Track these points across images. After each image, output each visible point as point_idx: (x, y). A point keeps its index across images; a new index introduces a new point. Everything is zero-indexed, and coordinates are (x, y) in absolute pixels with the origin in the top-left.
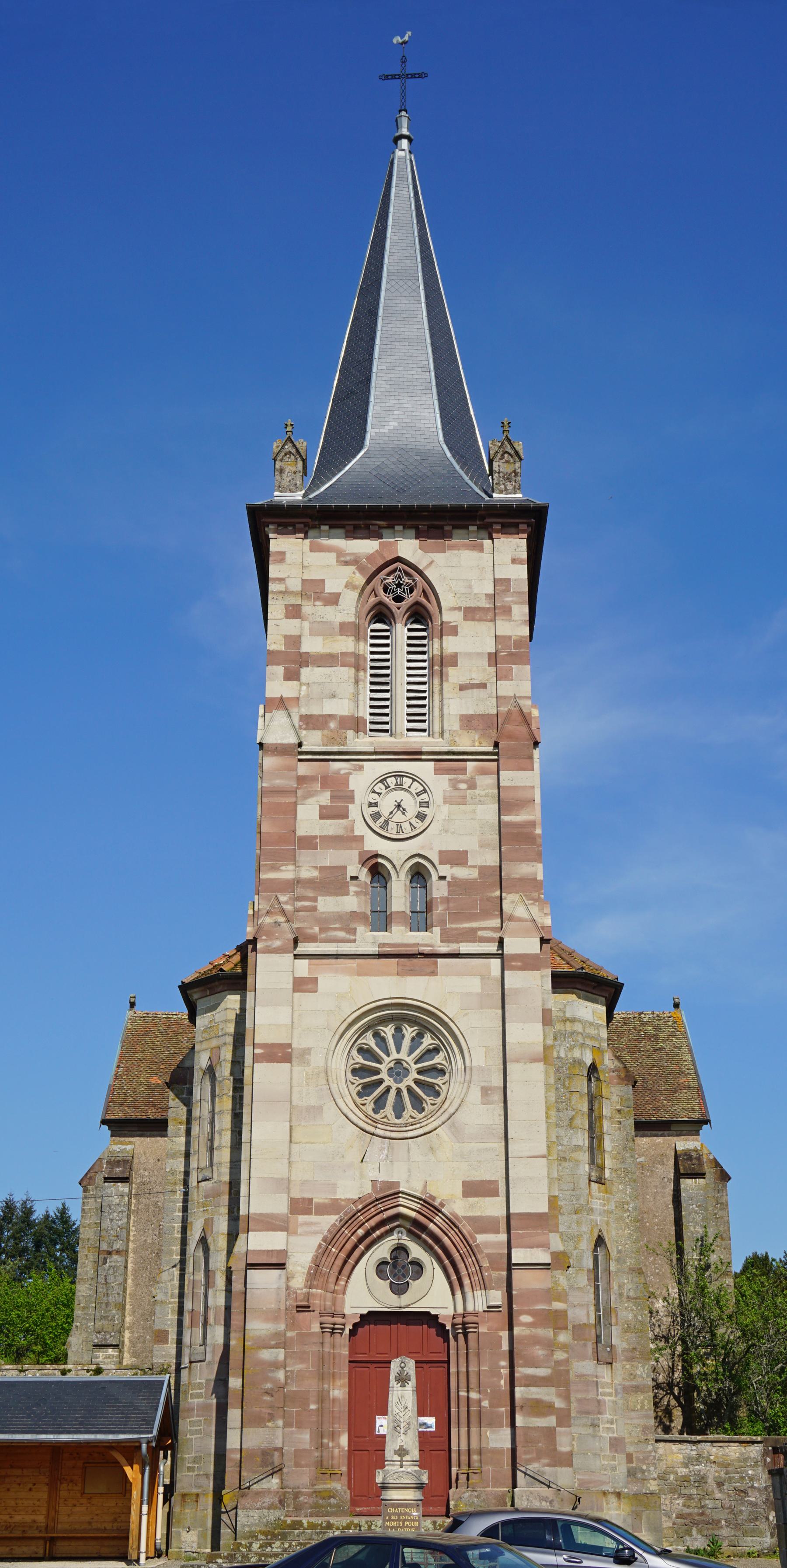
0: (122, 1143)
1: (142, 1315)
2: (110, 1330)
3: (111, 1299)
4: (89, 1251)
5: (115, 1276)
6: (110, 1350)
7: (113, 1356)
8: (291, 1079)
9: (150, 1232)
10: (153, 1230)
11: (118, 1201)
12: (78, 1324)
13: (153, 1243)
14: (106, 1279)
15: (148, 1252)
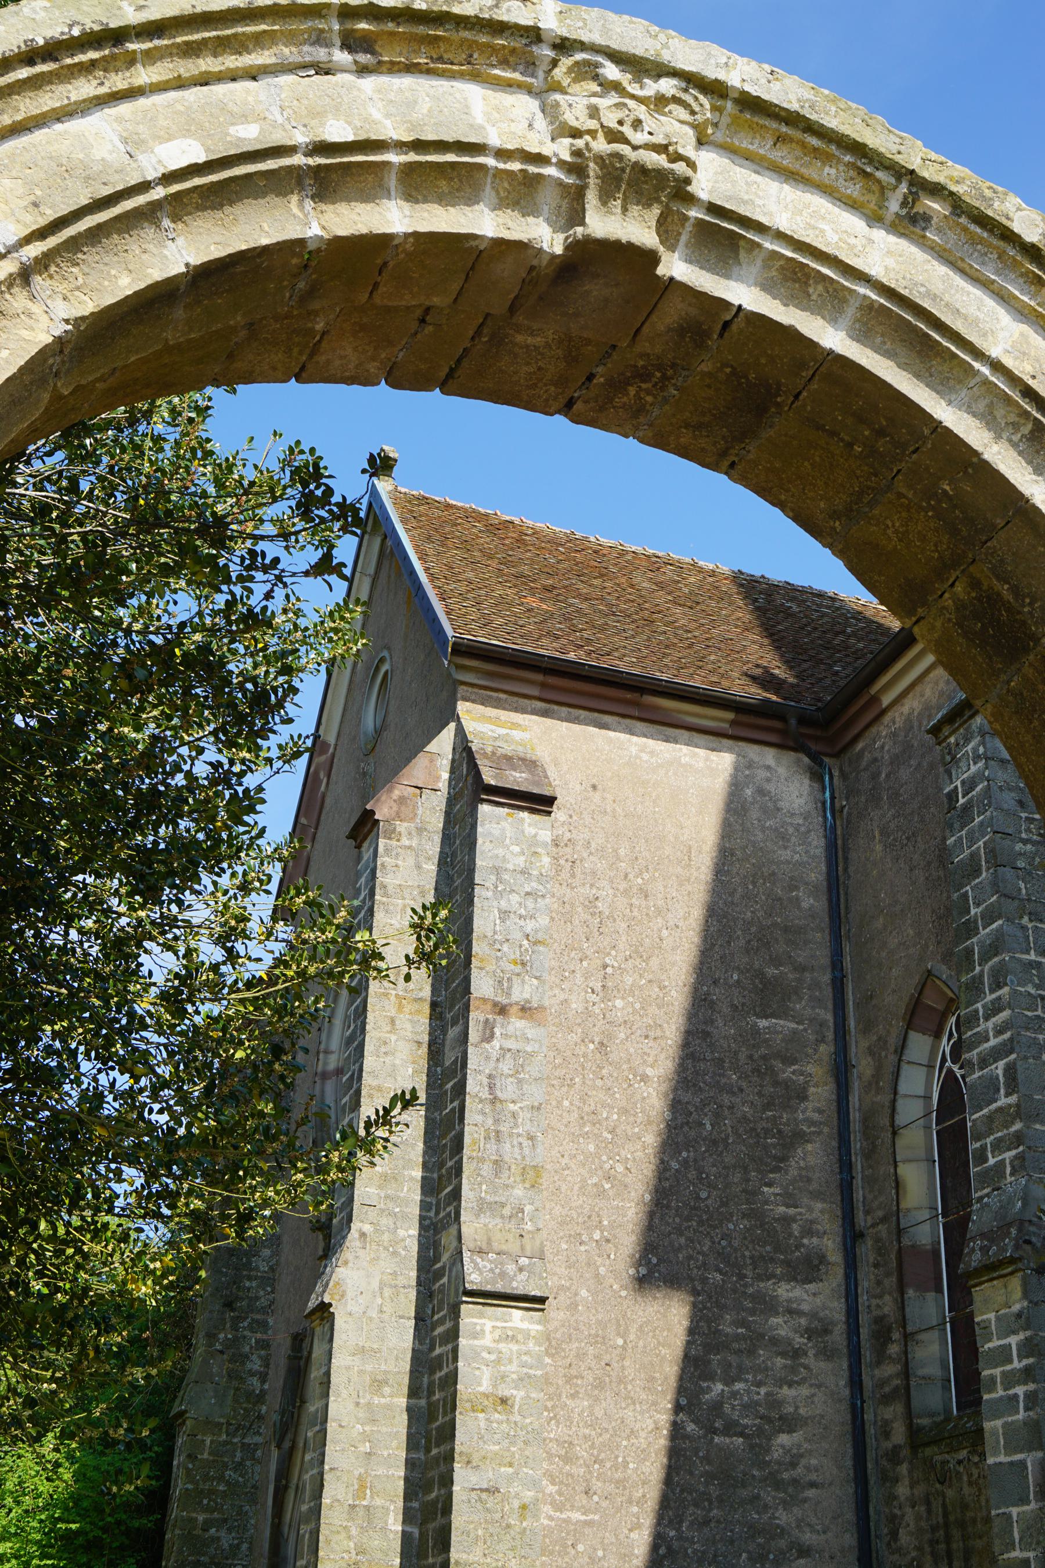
1: (562, 1224)
2: (513, 1247)
3: (509, 1151)
4: (400, 1008)
5: (520, 1081)
6: (517, 1314)
7: (527, 1334)
9: (579, 979)
10: (587, 976)
11: (521, 861)
12: (367, 1228)
13: (588, 1013)
14: (491, 1087)
15: (574, 1037)
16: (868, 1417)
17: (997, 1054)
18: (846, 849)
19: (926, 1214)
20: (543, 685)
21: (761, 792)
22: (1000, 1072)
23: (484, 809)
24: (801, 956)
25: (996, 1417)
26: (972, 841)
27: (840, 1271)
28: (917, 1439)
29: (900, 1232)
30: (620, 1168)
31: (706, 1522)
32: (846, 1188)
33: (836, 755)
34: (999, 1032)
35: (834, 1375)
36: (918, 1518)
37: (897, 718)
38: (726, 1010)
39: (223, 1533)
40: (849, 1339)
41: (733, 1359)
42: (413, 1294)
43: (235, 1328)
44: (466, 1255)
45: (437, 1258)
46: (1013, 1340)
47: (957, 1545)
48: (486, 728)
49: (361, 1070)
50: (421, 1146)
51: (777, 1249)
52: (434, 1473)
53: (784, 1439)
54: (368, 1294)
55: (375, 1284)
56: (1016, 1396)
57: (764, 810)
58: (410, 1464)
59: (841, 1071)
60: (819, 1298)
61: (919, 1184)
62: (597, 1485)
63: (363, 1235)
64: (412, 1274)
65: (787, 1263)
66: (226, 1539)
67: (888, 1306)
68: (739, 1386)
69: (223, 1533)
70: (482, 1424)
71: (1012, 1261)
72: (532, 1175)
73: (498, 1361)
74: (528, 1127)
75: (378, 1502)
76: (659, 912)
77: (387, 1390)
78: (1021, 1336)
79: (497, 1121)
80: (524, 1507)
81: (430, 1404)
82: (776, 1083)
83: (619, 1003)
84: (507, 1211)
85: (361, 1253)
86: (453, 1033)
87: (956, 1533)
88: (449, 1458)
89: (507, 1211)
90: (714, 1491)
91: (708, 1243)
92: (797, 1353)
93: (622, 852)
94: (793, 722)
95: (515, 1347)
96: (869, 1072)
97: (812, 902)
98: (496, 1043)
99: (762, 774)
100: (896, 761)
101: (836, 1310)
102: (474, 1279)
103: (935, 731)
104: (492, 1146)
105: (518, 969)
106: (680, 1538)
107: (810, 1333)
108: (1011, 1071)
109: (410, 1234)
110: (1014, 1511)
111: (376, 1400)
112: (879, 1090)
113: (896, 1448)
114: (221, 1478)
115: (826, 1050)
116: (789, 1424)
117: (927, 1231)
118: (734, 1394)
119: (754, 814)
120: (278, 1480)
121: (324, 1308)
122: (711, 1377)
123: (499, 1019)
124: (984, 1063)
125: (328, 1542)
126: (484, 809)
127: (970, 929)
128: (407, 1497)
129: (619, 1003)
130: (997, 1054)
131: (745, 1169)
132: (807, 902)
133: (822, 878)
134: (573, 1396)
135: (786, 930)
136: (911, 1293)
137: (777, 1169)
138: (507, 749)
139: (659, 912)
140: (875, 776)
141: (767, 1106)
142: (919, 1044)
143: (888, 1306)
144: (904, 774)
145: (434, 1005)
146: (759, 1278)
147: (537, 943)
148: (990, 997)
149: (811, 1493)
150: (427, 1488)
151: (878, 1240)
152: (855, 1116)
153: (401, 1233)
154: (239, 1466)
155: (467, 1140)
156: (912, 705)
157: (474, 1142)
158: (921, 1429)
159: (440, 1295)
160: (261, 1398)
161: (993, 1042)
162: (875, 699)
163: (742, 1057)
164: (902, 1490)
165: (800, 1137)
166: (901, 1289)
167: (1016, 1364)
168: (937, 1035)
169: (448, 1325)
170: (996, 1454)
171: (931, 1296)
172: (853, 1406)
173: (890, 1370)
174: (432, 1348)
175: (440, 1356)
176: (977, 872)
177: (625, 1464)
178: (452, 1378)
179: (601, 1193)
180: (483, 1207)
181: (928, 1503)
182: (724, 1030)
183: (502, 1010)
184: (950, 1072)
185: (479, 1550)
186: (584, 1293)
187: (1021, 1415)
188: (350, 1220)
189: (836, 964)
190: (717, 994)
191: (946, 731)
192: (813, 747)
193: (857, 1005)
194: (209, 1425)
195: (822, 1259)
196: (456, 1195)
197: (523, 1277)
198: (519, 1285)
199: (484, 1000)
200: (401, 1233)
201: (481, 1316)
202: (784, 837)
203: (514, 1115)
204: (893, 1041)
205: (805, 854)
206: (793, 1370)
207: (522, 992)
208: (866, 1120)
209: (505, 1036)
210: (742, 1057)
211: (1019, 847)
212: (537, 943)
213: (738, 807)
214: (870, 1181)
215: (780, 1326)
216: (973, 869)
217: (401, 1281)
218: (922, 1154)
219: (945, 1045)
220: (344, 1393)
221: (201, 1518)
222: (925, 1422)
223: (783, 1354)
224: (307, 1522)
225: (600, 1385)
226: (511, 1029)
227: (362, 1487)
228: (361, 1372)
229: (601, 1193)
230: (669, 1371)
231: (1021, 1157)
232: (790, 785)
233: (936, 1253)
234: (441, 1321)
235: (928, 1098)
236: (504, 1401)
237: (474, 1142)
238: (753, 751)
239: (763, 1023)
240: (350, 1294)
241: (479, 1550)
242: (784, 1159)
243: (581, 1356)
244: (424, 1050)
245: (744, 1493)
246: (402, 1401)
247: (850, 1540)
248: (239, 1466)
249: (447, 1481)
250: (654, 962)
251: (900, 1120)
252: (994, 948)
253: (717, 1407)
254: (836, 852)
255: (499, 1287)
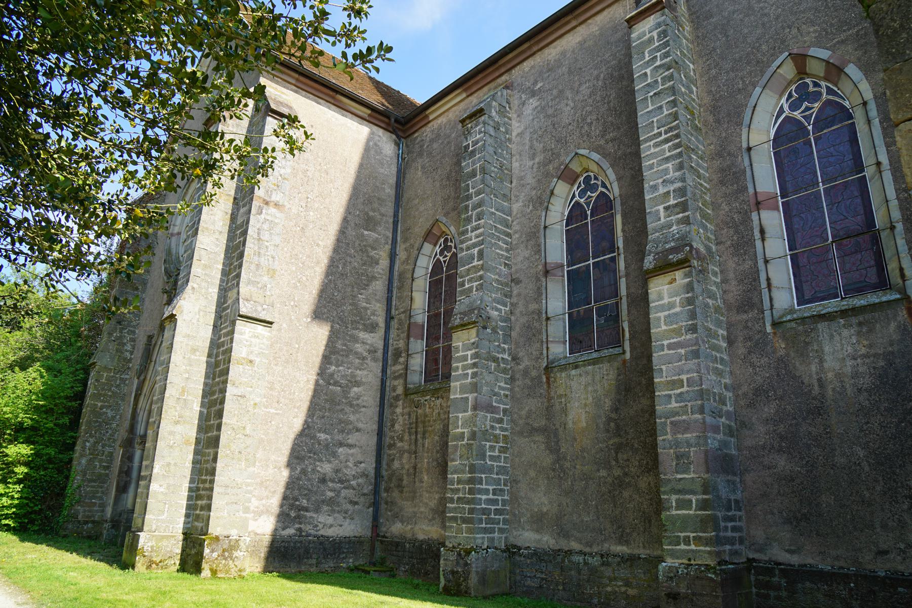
0: (276, 89)
2: (261, 300)
5: (271, 234)
8: (753, 113)
9: (297, 200)
12: (195, 286)
14: (259, 234)
15: (292, 224)
16: (388, 384)
17: (474, 245)
18: (405, 174)
19: (421, 311)
20: (297, 80)
21: (376, 144)
22: (476, 252)
23: (269, 119)
24: (383, 210)
25: (457, 381)
26: (474, 163)
27: (383, 330)
28: (407, 392)
29: (410, 316)
30: (304, 278)
31: (323, 417)
32: (389, 300)
33: (405, 138)
34: (477, 237)
35: (377, 368)
36: (405, 420)
37: (435, 125)
38: (353, 225)
39: (109, 411)
40: (384, 355)
41: (340, 358)
42: (213, 316)
43: (121, 332)
44: (241, 300)
45: (225, 302)
46: (469, 353)
47: (420, 430)
48: (272, 90)
49: (199, 219)
50: (223, 256)
51: (361, 319)
52: (217, 388)
53: (355, 389)
54: (194, 312)
55: (197, 310)
56: (467, 374)
57: (376, 152)
58: (205, 384)
59: (393, 256)
60: (375, 339)
61: (420, 301)
62: (282, 400)
63: (193, 288)
64: (213, 308)
65: (364, 325)
66: (110, 413)
67: (401, 344)
68: (341, 368)
69: (109, 411)
70: (241, 370)
71: (474, 322)
72: (272, 273)
73: (250, 345)
74: (272, 252)
75: (190, 398)
76: (331, 181)
77: (198, 353)
78: (473, 351)
79: (259, 248)
80: (255, 404)
81: (216, 361)
82: (368, 256)
83: (311, 213)
84: (259, 286)
85: (192, 296)
86: (242, 210)
87: (421, 425)
88: (225, 382)
89: (259, 286)
90: (327, 406)
91: (335, 313)
92: (364, 358)
93: (320, 154)
94: (393, 120)
95: (258, 341)
96: (404, 257)
97: (389, 191)
98: (263, 216)
99: (377, 138)
100: (432, 141)
101: (380, 345)
102: (243, 310)
103: (462, 121)
104: (256, 258)
105: (275, 188)
106: (313, 422)
107: (370, 352)
108: (481, 253)
109: (214, 292)
110: (460, 415)
111: (193, 357)
112: (408, 264)
113: (398, 396)
114: (110, 390)
115: (388, 247)
116: (358, 384)
117: (421, 316)
118: (339, 371)
119: (372, 152)
120: (137, 391)
121: (172, 317)
122: (331, 364)
123: (265, 206)
124: (468, 249)
125: (166, 412)
126: (269, 119)
127: (469, 197)
128: (203, 397)
129: (311, 213)
130: (474, 245)
131: (353, 287)
132: (388, 190)
133: (394, 182)
134: (276, 365)
135: (379, 199)
136: (412, 339)
137: (365, 289)
138: (281, 100)
139: (331, 181)
140: (422, 146)
141: (364, 264)
142: (427, 248)
143: (401, 344)
144: (435, 146)
145: (235, 199)
146: (353, 329)
147: (285, 179)
148: (474, 224)
149: (363, 409)
150: (213, 393)
151: (400, 320)
152: (396, 274)
153: (210, 290)
154: (118, 386)
155: (246, 253)
156: (443, 120)
157: (249, 255)
158: (409, 389)
159: (226, 316)
160: (130, 360)
161: (473, 241)
162: (427, 116)
163: (357, 244)
164: (399, 410)
165: (374, 278)
166: (408, 337)
167: (469, 362)
168: (435, 245)
169: (229, 329)
170: (455, 393)
171: (419, 341)
172: (382, 379)
173: (398, 367)
174: (220, 338)
175: (223, 342)
176: (475, 176)
177: (294, 393)
178: (230, 350)
179: (296, 287)
180: (249, 282)
181: (410, 415)
182: (351, 232)
183: (267, 203)
184: (438, 259)
185: (235, 419)
186: (284, 325)
187: (469, 380)
188: (188, 281)
189: (396, 215)
190: (350, 217)
191: (467, 122)
192: (400, 133)
193: (402, 232)
194: (106, 369)
195: (377, 325)
196: (238, 276)
197: (265, 312)
198: (262, 316)
199: (260, 197)
200: (210, 290)
201: (245, 326)
202: (382, 164)
203: (267, 247)
204: (417, 246)
205: (389, 172)
206: (362, 364)
207: (276, 197)
208: (401, 275)
209: (267, 214)
210: (357, 244)
211: (493, 168)
212: (285, 179)
213: (369, 149)
214: (399, 298)
215: (359, 347)
216: (473, 174)
217: (208, 310)
218: (422, 289)
219: (438, 249)
220: (179, 353)
221: (99, 404)
222: (411, 386)
223: (359, 358)
224: (156, 403)
225: (287, 362)
226: (270, 211)
227: (183, 391)
228: (187, 345)
229: (296, 287)
230: (317, 360)
231: (481, 285)
232: (387, 145)
233: (423, 326)
234: (225, 328)
235: (428, 268)
236: (251, 362)
237: (249, 255)
238: (375, 128)
239: (366, 233)
240: (185, 312)
241: (235, 419)
242: (367, 285)
243: (281, 350)
244: (229, 216)
245: (338, 408)
246: (205, 359)
247: (375, 427)
248: (118, 386)
249: (223, 391)
250: (327, 200)
251: (415, 276)
252: (479, 205)
253: (332, 375)
254: (401, 174)
255: (254, 315)
